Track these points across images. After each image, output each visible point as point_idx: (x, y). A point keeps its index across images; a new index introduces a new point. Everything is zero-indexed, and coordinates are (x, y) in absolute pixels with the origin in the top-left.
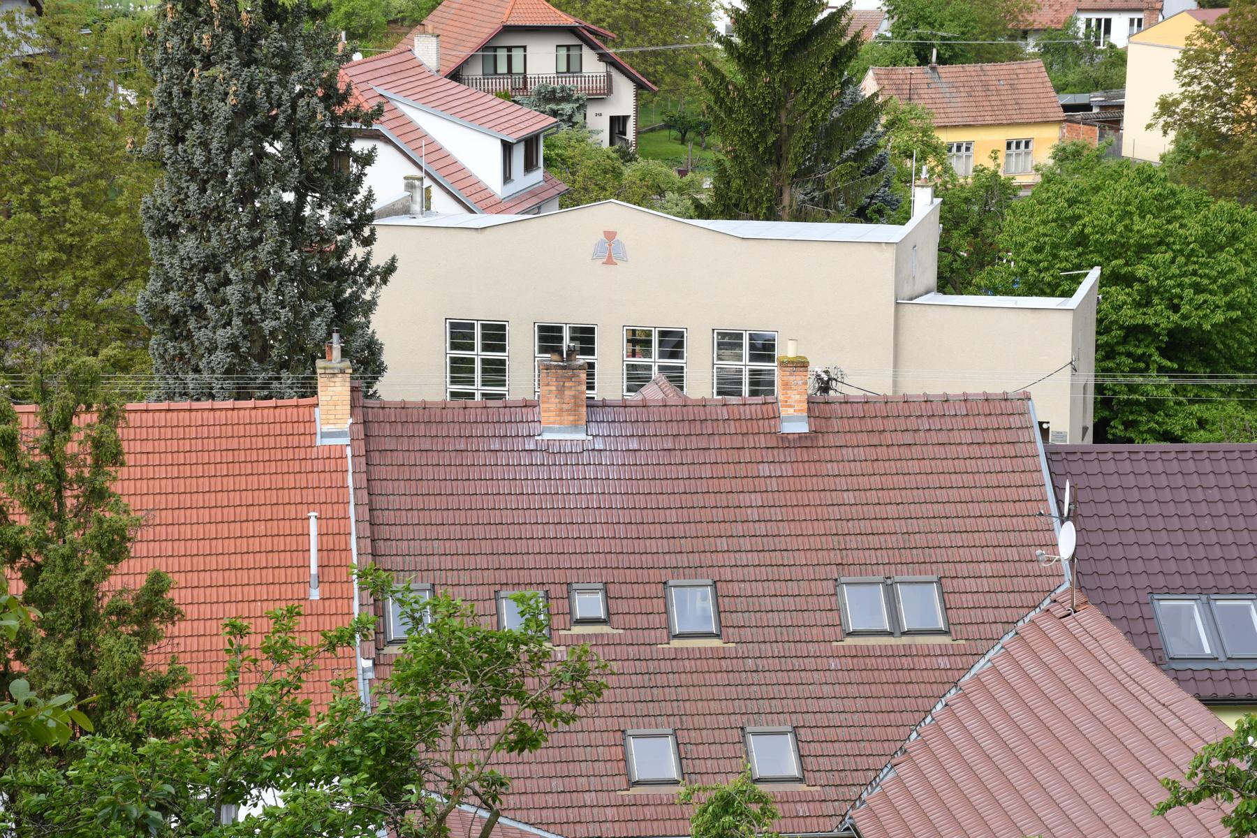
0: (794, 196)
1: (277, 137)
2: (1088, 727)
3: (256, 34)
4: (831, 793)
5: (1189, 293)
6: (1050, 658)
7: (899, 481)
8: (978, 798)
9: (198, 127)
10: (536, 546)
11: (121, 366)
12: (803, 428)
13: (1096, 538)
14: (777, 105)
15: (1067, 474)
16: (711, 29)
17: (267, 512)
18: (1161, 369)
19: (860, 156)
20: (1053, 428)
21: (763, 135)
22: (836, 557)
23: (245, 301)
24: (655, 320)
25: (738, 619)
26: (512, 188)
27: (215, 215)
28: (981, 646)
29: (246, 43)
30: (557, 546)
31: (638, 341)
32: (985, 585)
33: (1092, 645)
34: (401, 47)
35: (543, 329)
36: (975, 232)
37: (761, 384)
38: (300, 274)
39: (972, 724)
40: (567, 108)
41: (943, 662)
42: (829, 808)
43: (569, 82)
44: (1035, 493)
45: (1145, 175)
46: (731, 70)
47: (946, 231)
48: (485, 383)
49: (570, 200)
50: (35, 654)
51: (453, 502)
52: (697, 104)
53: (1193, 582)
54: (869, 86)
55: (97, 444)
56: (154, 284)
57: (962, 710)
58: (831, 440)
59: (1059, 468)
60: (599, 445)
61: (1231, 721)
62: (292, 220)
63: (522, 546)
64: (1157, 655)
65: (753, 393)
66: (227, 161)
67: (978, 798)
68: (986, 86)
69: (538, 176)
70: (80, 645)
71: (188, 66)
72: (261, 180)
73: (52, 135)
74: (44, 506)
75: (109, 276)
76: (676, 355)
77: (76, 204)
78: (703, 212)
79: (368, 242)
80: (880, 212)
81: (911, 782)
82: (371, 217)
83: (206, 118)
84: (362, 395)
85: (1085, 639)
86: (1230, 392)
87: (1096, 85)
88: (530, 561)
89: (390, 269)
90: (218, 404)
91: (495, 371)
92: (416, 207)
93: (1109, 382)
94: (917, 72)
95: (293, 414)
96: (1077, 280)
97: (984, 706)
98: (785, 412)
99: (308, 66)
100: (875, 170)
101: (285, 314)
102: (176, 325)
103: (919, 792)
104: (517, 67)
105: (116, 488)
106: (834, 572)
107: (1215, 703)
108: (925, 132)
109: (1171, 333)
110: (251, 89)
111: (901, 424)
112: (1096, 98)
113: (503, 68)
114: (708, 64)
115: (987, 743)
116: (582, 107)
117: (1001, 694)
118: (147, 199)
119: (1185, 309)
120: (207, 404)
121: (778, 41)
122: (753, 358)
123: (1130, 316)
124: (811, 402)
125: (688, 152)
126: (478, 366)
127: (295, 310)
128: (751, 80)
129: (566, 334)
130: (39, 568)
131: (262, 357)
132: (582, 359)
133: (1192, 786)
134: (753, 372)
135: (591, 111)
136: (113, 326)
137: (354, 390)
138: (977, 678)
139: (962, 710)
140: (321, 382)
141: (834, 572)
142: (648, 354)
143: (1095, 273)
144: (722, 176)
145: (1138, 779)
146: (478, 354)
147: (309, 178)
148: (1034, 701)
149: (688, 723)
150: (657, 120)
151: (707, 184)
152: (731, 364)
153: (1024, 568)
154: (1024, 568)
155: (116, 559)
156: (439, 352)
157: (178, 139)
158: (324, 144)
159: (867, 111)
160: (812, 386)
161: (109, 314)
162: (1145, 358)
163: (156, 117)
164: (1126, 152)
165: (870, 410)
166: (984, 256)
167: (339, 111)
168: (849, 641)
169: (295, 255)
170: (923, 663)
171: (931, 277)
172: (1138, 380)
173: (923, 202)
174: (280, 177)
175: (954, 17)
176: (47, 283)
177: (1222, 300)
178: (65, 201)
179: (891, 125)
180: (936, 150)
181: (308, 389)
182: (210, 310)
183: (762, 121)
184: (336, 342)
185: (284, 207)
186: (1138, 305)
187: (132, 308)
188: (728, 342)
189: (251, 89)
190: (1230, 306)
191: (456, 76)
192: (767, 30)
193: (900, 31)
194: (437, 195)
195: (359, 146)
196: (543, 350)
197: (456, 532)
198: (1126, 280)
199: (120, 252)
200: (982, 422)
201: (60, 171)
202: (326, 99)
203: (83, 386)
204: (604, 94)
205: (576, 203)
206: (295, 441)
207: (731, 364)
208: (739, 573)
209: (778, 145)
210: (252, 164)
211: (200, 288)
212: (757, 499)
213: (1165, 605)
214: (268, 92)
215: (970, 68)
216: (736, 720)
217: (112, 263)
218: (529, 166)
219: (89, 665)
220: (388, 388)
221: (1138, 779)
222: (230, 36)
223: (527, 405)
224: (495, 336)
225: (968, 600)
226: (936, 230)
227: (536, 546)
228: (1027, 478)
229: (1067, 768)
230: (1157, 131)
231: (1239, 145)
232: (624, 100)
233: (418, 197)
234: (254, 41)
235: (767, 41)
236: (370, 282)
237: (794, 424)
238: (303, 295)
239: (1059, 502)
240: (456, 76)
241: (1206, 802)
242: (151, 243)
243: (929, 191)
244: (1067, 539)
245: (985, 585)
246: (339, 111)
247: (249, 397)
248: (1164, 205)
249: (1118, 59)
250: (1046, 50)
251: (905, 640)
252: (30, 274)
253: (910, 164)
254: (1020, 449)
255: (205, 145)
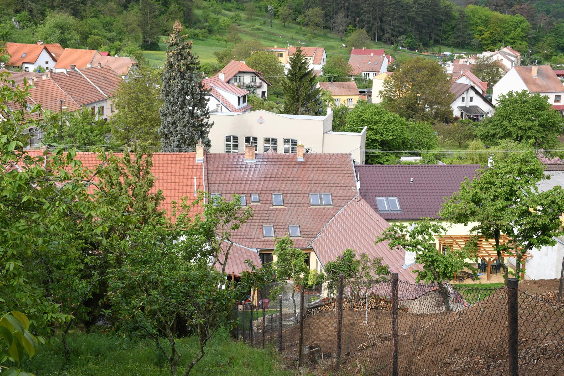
0: (301, 109)
1: (189, 95)
2: (361, 225)
3: (185, 73)
4: (307, 239)
5: (385, 132)
6: (354, 210)
7: (323, 172)
8: (338, 240)
9: (172, 93)
10: (243, 185)
11: (153, 144)
12: (302, 160)
13: (365, 185)
14: (298, 90)
15: (359, 171)
16: (284, 73)
17: (185, 177)
18: (379, 149)
19: (316, 101)
20: (356, 161)
21: (295, 96)
22: (309, 188)
23: (181, 131)
24: (271, 137)
25: (287, 202)
26: (240, 107)
27: (176, 112)
28: (340, 208)
29: (183, 75)
30: (248, 185)
31: (267, 141)
32: (341, 195)
33: (363, 208)
34: (216, 76)
35: (246, 138)
36: (340, 118)
37: (293, 151)
38: (193, 125)
39: (337, 225)
40: (252, 89)
41: (332, 211)
42: (306, 242)
43: (253, 84)
44: (352, 175)
45: (376, 107)
46: (288, 82)
47: (334, 118)
48: (233, 149)
49: (253, 109)
50: (134, 207)
51: (226, 175)
52: (281, 89)
53: (395, 194)
54: (318, 86)
55: (147, 162)
56: (162, 127)
57: (335, 222)
58: (308, 163)
59: (357, 170)
60: (258, 163)
61: (391, 224)
62: (191, 113)
63: (240, 185)
64: (376, 210)
65: (292, 152)
66: (178, 100)
67: (338, 240)
68: (343, 87)
69: (246, 104)
70: (143, 205)
71: (170, 80)
72: (185, 105)
73: (140, 95)
74: (136, 175)
75: (152, 125)
76: (275, 144)
77: (145, 109)
78: (281, 113)
79: (208, 118)
80: (320, 113)
81: (324, 237)
82: (209, 113)
83: (173, 91)
84: (206, 152)
85: (362, 207)
86: (394, 153)
87: (366, 87)
88: (242, 189)
89: (213, 124)
90: (175, 153)
91: (235, 146)
92: (219, 111)
93: (368, 151)
94: (328, 83)
95: (191, 156)
96: (362, 129)
97: (340, 221)
98: (298, 157)
99: (195, 80)
100: (319, 104)
101: (190, 134)
102: (166, 136)
103: (326, 239)
104: (242, 81)
105: (150, 171)
106: (308, 192)
107: (388, 220)
108: (330, 96)
109: (381, 141)
110: (183, 85)
111: (324, 160)
112: (366, 90)
113: (238, 81)
114: (283, 80)
115: (340, 229)
116: (256, 89)
117: (344, 218)
118: (161, 108)
119: (384, 136)
120: (172, 153)
121: (298, 76)
122: (292, 145)
123: (373, 137)
124: (304, 155)
125: (279, 99)
126: (232, 146)
127: (192, 133)
128: (292, 84)
129: (251, 139)
130: (135, 188)
131: (185, 143)
132: (254, 144)
133: (382, 237)
134: (292, 148)
135: (257, 90)
136: (153, 136)
137: (204, 150)
138: (339, 215)
139: (335, 222)
140: (197, 149)
141: (308, 192)
142: (269, 143)
143: (366, 128)
144: (286, 105)
145: (371, 236)
146: (232, 143)
147: (196, 104)
148: (351, 220)
149: (276, 224)
150: (272, 92)
151: (283, 106)
152: (287, 146)
153: (349, 191)
154: (349, 191)
155: (151, 186)
156: (223, 143)
157: (167, 95)
158: (199, 97)
159: (318, 91)
160: (304, 151)
161: (152, 133)
162: (375, 146)
163: (163, 91)
164: (373, 102)
165: (317, 157)
166: (342, 123)
167: (202, 90)
168: (312, 207)
169: (192, 121)
170: (327, 211)
171: (331, 128)
172: (374, 151)
173: (329, 112)
174: (189, 104)
175: (336, 72)
176: (139, 126)
177: (392, 134)
178: (143, 109)
179: (323, 94)
180: (332, 100)
181: (194, 150)
182: (174, 133)
183: (294, 93)
184: (201, 140)
185: (190, 110)
186: (375, 135)
187: (157, 132)
188: (287, 141)
189: (183, 85)
190: (393, 135)
191: (228, 82)
192: (296, 73)
193: (325, 74)
194: (224, 108)
195: (206, 97)
196: (246, 142)
197: (226, 182)
198: (372, 129)
199: (155, 120)
200: (341, 160)
201: (142, 102)
202: (199, 87)
203: (144, 149)
204: (260, 87)
205: (254, 110)
206: (191, 161)
207: (287, 146)
208: (288, 192)
209: (298, 98)
210: (183, 101)
211: (171, 128)
212: (292, 176)
213: (378, 199)
214: (187, 86)
215: (340, 83)
216: (287, 224)
217: (153, 122)
218: (244, 102)
219: (145, 209)
220: (212, 150)
221: (371, 236)
222: (179, 73)
223: (242, 154)
224: (236, 139)
225: (337, 198)
226: (332, 117)
227: (243, 185)
228: (350, 172)
229: (357, 234)
230: (379, 97)
231: (396, 101)
232: (265, 88)
233: (219, 108)
234: (184, 74)
235: (296, 76)
236: (208, 127)
237: (301, 159)
238: (194, 130)
239: (357, 177)
240: (228, 82)
241: (385, 241)
242: (161, 118)
243: (330, 109)
244: (358, 185)
245: (341, 195)
246: (202, 90)
247: (181, 152)
248: (379, 113)
249: (371, 82)
250: (356, 79)
251: (324, 207)
252: (136, 124)
253: (327, 103)
254: (349, 165)
255: (173, 97)
